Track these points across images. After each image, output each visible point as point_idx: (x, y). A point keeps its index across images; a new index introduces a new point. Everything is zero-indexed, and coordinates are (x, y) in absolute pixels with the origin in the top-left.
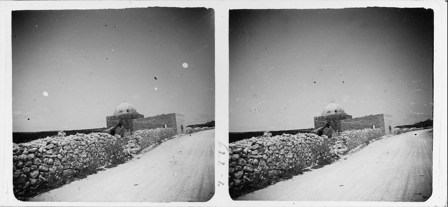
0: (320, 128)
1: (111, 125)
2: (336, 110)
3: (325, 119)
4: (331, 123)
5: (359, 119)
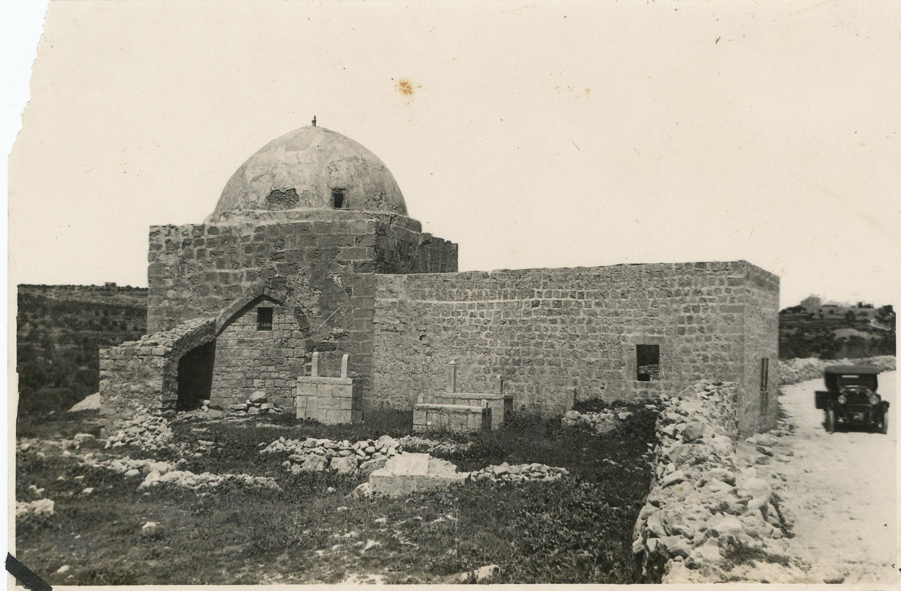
0: (193, 324)
1: (184, 301)
2: (341, 185)
3: (241, 250)
4: (290, 291)
5: (536, 283)
